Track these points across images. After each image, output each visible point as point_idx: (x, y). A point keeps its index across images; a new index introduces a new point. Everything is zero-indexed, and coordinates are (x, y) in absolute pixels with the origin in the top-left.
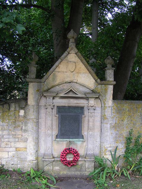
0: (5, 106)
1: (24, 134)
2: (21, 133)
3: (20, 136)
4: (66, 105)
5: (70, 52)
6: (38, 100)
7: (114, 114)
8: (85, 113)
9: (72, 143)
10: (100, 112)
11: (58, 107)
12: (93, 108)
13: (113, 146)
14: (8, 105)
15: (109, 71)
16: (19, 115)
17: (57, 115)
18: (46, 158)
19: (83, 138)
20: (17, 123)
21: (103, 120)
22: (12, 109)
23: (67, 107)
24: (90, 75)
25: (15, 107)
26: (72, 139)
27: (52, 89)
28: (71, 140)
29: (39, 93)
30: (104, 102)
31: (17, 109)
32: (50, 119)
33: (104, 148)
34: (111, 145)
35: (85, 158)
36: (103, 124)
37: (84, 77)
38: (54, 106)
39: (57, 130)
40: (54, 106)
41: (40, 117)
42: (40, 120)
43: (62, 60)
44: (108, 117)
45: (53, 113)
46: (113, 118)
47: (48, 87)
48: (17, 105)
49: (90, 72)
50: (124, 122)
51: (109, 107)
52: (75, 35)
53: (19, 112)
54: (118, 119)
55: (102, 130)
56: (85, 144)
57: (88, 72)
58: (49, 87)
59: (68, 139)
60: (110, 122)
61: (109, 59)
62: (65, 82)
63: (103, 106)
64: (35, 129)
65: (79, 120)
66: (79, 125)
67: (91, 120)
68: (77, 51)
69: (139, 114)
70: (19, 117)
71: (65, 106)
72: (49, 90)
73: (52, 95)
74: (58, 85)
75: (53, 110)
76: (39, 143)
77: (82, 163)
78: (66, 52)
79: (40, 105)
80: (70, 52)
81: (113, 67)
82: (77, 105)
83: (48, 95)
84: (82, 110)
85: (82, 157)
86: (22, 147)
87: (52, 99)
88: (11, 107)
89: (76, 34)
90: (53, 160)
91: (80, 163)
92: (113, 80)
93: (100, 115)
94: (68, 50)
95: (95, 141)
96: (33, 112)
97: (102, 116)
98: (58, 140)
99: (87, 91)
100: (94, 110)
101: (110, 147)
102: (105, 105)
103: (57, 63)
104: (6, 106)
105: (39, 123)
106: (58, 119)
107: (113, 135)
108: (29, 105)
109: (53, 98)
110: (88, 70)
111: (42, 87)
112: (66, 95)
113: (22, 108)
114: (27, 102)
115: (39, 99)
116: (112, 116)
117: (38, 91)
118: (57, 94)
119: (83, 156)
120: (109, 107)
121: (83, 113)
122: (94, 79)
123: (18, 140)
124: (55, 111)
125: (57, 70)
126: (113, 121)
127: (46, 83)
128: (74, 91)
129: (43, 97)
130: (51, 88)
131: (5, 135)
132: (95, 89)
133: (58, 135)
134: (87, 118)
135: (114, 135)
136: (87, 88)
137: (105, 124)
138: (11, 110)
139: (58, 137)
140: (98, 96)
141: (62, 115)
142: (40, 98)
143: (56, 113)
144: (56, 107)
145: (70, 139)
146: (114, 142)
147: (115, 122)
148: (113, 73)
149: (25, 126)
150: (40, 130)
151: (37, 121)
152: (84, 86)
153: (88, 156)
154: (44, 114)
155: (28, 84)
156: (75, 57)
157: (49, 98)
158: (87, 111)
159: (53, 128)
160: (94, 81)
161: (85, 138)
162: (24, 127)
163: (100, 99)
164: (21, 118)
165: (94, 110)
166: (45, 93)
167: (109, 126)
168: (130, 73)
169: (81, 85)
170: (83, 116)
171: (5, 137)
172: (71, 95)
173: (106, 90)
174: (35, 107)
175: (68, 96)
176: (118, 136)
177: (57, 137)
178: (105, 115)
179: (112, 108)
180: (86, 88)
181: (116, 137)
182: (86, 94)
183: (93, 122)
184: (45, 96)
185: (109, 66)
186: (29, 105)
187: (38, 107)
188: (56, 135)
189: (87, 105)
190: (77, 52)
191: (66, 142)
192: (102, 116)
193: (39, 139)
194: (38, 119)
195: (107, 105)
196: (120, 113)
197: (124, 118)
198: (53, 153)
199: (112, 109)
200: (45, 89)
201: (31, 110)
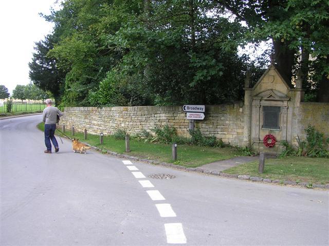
22: (235, 107)
58: (257, 93)
104: (232, 105)
109: (260, 101)
113: (241, 107)
118: (262, 98)
121: (280, 111)
124: (261, 109)
125: (262, 82)
134: (282, 115)
144: (262, 107)
149: (243, 118)
167: (297, 121)
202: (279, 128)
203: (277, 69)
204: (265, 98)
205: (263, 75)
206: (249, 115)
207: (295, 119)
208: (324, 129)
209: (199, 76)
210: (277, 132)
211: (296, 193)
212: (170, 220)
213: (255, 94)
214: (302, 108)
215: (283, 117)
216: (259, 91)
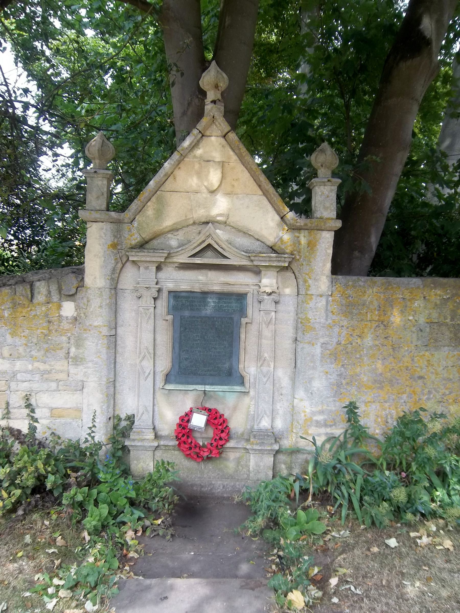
0: (20, 289)
1: (73, 370)
2: (65, 368)
3: (62, 376)
4: (197, 288)
5: (208, 133)
6: (114, 270)
7: (334, 317)
8: (249, 311)
9: (211, 397)
10: (293, 309)
11: (172, 294)
12: (273, 297)
13: (331, 411)
14: (29, 287)
15: (322, 187)
16: (60, 316)
17: (170, 317)
18: (134, 440)
19: (242, 383)
20: (55, 338)
21: (300, 334)
22: (40, 298)
23: (199, 295)
24: (265, 201)
25: (49, 292)
26: (212, 384)
27: (155, 243)
28: (208, 388)
29: (115, 251)
30: (305, 281)
31: (55, 298)
32: (150, 327)
33: (303, 415)
34: (325, 407)
35: (248, 440)
36: (300, 346)
37: (248, 207)
38: (159, 291)
39: (169, 360)
40: (159, 291)
41: (120, 322)
42: (120, 331)
43: (183, 157)
44: (317, 326)
45: (158, 310)
46: (330, 327)
47: (144, 236)
48: (54, 288)
49: (265, 193)
50: (365, 340)
51: (321, 296)
52: (223, 77)
53: (60, 307)
54: (344, 332)
55: (298, 362)
56: (247, 400)
57: (261, 193)
58: (146, 235)
59: (200, 386)
60: (322, 340)
61: (323, 151)
62: (191, 222)
63: (302, 292)
64: (104, 356)
65: (232, 333)
66: (231, 345)
67: (267, 333)
68: (226, 127)
69: (411, 318)
70: (60, 322)
71: (191, 292)
72: (147, 246)
73: (154, 259)
74: (174, 230)
75: (159, 302)
76: (117, 396)
77: (238, 455)
78: (195, 131)
79: (120, 286)
80: (208, 133)
81: (334, 174)
82: (226, 289)
83: (143, 259)
84: (241, 303)
85: (241, 437)
86: (68, 406)
87: (96, 508)
88: (36, 294)
89: (224, 75)
90: (156, 444)
91: (232, 456)
92: (335, 216)
93: (292, 319)
94: (204, 121)
95: (276, 394)
96: (101, 307)
97: (299, 320)
98: (170, 387)
99: (256, 246)
100: (276, 303)
101: (321, 412)
102: (307, 289)
103: (267, 188)
104: (22, 290)
105: (118, 338)
106: (171, 328)
107: (329, 376)
108: (88, 288)
109: (159, 268)
110: (260, 186)
111: (126, 234)
112: (198, 261)
113: (71, 297)
114: (83, 278)
115: (118, 271)
116: (330, 321)
117: (114, 246)
118: (169, 256)
119: (242, 434)
120: (321, 296)
121: (242, 312)
122: (278, 212)
123: (58, 387)
124: (162, 304)
125: (169, 185)
126: (330, 336)
127: (135, 224)
128: (216, 247)
129: (128, 265)
130: (151, 240)
131: (19, 372)
132: (279, 243)
133: (172, 373)
134: (253, 329)
135: (333, 378)
136: (258, 240)
137: (306, 346)
138: (35, 301)
139: (173, 378)
140: (286, 265)
141: (182, 318)
142: (120, 265)
143: (165, 310)
144: (165, 294)
145: (205, 384)
146: (331, 399)
147: (335, 340)
148: (333, 196)
149: (78, 346)
150: (119, 359)
151: (113, 333)
152: (245, 233)
153: (255, 437)
154: (133, 314)
155: (85, 229)
156: (223, 146)
157: (147, 268)
158: (256, 304)
159: (158, 352)
160: (277, 218)
161: (247, 385)
162: (73, 350)
163: (294, 272)
164: (65, 325)
165: (276, 303)
166: (133, 253)
167: (318, 350)
168: (390, 195)
169: (239, 231)
170: (244, 321)
171: (19, 376)
172: (208, 259)
173: (311, 245)
174: (106, 294)
175: (199, 262)
176: (344, 382)
177: (168, 379)
178: (308, 320)
179: (330, 299)
180: (254, 241)
181: (339, 385)
182: (252, 258)
183: (274, 337)
184: (133, 261)
185: (323, 173)
186: (88, 288)
187: (116, 294)
188: (165, 372)
189: (257, 287)
190: (226, 131)
191: (194, 392)
192: (299, 320)
193: (117, 385)
194: (116, 328)
195: (313, 291)
196: (351, 313)
197: (366, 330)
198: (157, 423)
199: (327, 302)
200: (134, 242)
201: (96, 302)
202: (241, 381)
203: (424, 37)
204: (183, 259)
205: (176, 156)
206: (105, 331)
207: (312, 344)
208: (421, 378)
209: (310, 499)
210: (231, 399)
211: (114, 402)
212: (84, 18)
213: (135, 239)
214: (337, 296)
215: (260, 335)
216: (158, 228)
